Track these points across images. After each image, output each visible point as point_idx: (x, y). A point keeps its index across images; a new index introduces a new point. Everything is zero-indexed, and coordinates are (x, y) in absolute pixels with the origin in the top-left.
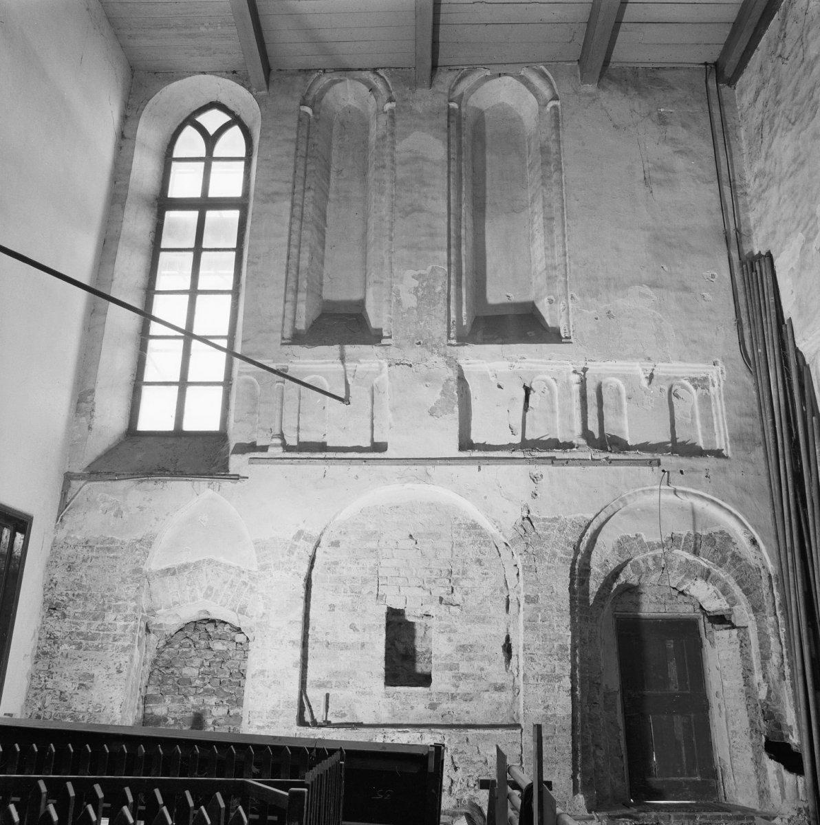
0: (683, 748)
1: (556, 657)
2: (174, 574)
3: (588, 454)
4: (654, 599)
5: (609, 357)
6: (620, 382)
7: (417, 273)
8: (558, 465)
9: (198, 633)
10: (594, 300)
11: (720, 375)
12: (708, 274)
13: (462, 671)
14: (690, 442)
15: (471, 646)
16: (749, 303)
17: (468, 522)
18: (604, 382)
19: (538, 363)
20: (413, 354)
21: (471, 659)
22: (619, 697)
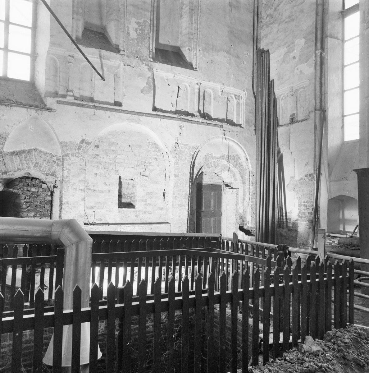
0: (213, 229)
1: (184, 198)
2: (17, 154)
3: (200, 120)
4: (209, 177)
5: (210, 81)
6: (211, 91)
7: (137, 21)
8: (190, 123)
9: (22, 183)
10: (207, 53)
11: (245, 96)
12: (246, 53)
13: (148, 202)
14: (231, 120)
15: (152, 193)
16: (258, 69)
17: (153, 142)
18: (206, 90)
19: (185, 77)
20: (135, 62)
21: (151, 198)
22: (195, 212)
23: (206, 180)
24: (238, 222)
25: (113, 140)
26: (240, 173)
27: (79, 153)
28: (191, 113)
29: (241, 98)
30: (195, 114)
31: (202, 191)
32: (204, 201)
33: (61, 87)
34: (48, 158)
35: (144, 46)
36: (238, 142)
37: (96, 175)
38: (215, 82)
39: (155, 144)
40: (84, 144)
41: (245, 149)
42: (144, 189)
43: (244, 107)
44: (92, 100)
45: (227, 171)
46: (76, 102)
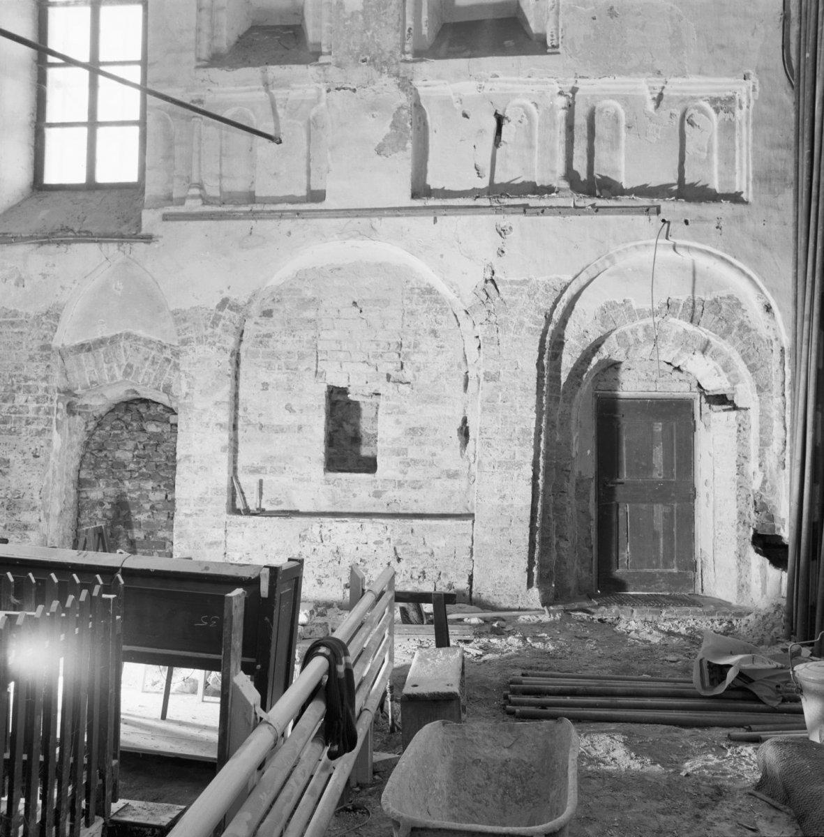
1: (516, 442)
2: (89, 350)
3: (568, 200)
4: (643, 376)
5: (606, 73)
6: (616, 105)
8: (531, 214)
11: (751, 94)
13: (410, 456)
15: (422, 429)
17: (423, 286)
18: (599, 106)
20: (358, 74)
21: (421, 443)
22: (593, 484)
23: (630, 386)
24: (747, 519)
25: (309, 294)
26: (746, 358)
27: (213, 335)
28: (542, 187)
29: (738, 104)
30: (555, 185)
31: (616, 420)
32: (624, 452)
33: (177, 181)
34: (153, 353)
35: (386, 24)
36: (725, 251)
37: (265, 386)
38: (627, 73)
39: (430, 291)
40: (227, 310)
41: (759, 273)
42: (397, 420)
43: (751, 131)
44: (251, 198)
45: (698, 354)
46: (208, 209)
